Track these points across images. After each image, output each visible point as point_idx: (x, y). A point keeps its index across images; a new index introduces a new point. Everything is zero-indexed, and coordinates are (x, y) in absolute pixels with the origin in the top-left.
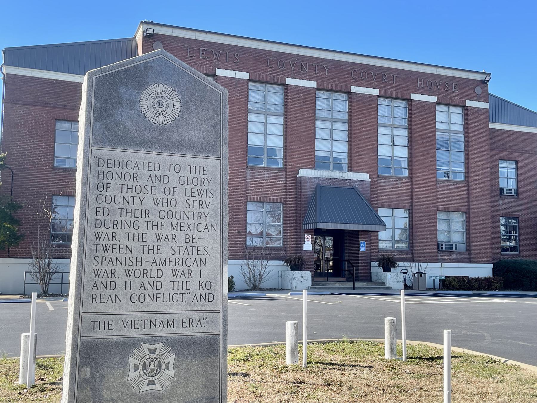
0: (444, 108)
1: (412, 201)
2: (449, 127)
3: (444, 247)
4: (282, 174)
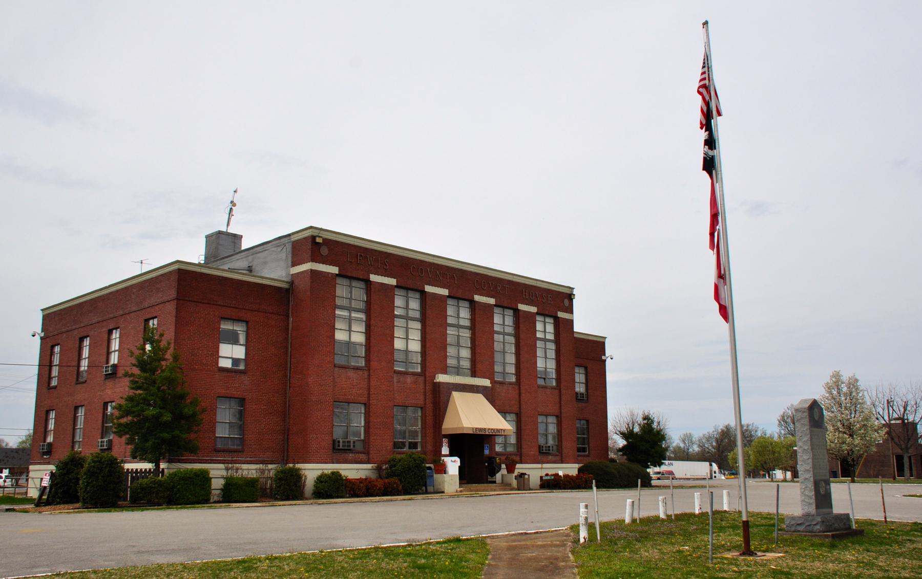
0: (345, 282)
1: (369, 394)
2: (407, 313)
3: (341, 444)
4: (421, 379)
